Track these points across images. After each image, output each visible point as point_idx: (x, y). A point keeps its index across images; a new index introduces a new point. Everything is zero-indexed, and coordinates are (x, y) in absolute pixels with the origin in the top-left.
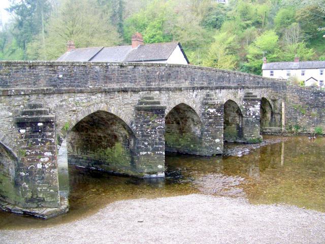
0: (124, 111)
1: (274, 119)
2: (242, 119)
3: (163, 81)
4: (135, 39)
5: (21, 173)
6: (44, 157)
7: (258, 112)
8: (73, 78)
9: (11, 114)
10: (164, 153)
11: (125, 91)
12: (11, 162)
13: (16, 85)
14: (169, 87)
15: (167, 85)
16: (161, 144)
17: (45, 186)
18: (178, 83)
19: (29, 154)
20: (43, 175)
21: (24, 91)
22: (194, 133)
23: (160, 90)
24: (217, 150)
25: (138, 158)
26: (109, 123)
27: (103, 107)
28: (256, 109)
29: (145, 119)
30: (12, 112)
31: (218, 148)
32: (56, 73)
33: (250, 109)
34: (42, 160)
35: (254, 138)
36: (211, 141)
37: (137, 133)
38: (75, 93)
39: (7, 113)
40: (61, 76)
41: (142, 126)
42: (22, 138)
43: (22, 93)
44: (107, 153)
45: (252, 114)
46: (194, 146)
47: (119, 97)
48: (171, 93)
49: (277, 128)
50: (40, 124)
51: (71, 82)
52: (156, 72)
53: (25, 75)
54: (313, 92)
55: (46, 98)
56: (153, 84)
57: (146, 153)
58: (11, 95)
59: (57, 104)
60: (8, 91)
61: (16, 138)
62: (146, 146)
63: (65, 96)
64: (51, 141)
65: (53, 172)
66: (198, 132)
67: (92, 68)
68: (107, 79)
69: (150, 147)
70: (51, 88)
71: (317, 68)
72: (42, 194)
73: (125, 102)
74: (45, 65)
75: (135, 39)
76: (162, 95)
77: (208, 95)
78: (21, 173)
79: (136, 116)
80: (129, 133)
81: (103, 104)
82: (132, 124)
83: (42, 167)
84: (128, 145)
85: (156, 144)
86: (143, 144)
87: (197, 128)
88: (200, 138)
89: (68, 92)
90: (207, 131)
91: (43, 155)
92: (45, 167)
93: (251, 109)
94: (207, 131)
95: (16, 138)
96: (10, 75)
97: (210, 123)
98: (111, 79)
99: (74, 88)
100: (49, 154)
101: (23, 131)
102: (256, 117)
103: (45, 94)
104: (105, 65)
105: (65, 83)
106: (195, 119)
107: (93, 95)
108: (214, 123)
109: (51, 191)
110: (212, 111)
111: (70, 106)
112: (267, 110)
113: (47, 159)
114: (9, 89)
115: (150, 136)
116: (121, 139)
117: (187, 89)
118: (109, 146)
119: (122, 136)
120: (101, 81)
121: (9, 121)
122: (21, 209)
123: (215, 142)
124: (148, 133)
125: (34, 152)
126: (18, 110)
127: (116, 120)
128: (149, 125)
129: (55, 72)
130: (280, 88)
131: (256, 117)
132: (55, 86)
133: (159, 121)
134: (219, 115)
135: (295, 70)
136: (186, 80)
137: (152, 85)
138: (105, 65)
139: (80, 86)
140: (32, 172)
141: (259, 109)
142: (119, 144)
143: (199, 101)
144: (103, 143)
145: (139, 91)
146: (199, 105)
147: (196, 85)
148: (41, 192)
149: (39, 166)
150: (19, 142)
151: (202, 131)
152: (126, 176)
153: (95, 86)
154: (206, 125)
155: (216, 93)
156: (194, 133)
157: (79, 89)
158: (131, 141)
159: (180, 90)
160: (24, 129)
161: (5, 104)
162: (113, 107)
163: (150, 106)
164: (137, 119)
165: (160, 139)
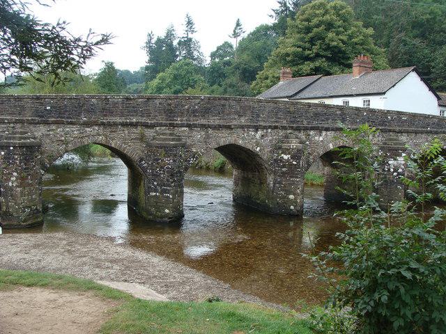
3: (195, 116)
14: (207, 123)
33: (390, 162)
34: (12, 179)
38: (63, 124)
45: (392, 170)
48: (210, 131)
50: (12, 148)
52: (183, 106)
55: (31, 127)
71: (393, 86)
76: (195, 133)
89: (54, 123)
93: (391, 162)
94: (280, 183)
97: (284, 173)
110: (286, 157)
113: (14, 178)
123: (288, 198)
147: (262, 123)
159: (229, 127)
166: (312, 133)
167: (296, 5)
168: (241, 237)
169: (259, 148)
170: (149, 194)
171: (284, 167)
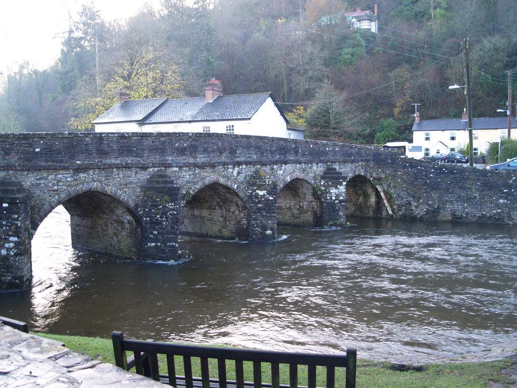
0: (125, 192)
6: (10, 242)
11: (127, 167)
27: (95, 185)
34: (7, 245)
37: (144, 219)
41: (150, 210)
45: (334, 198)
64: (17, 224)
68: (102, 153)
77: (257, 172)
81: (96, 184)
85: (168, 233)
89: (47, 169)
93: (333, 191)
97: (259, 209)
99: (56, 164)
100: (15, 239)
110: (261, 193)
111: (50, 185)
112: (369, 193)
113: (12, 245)
127: (118, 203)
129: (30, 145)
133: (171, 205)
134: (271, 198)
141: (344, 190)
155: (273, 169)
157: (62, 165)
166: (275, 167)
168: (29, 180)
169: (236, 186)
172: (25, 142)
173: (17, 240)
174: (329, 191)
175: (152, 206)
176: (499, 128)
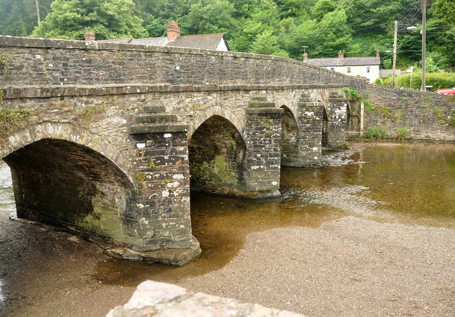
1: (350, 123)
2: (327, 123)
3: (269, 78)
4: (171, 30)
5: (138, 205)
6: (172, 180)
7: (345, 114)
8: (189, 72)
9: (125, 121)
10: (279, 167)
11: (237, 90)
12: (119, 190)
13: (131, 80)
15: (272, 84)
16: (277, 155)
17: (173, 221)
18: (281, 81)
19: (150, 177)
20: (171, 206)
21: (141, 89)
22: (288, 140)
23: (267, 89)
24: (315, 160)
25: (249, 174)
26: (212, 131)
28: (342, 111)
29: (258, 125)
30: (125, 118)
31: (316, 158)
32: (173, 64)
33: (336, 111)
34: (169, 185)
35: (339, 144)
36: (309, 150)
39: (120, 120)
40: (178, 68)
42: (140, 155)
43: (138, 91)
44: (202, 168)
45: (337, 117)
46: (287, 156)
47: (232, 97)
49: (355, 133)
50: (167, 136)
51: (188, 77)
52: (264, 66)
53: (140, 65)
54: (395, 92)
56: (261, 81)
57: (258, 167)
58: (125, 94)
59: (175, 106)
60: (122, 87)
61: (131, 156)
62: (258, 159)
63: (183, 96)
65: (185, 201)
66: (293, 139)
67: (208, 59)
69: (263, 160)
70: (167, 84)
71: (363, 65)
72: (168, 232)
73: (238, 104)
74: (162, 51)
75: (171, 30)
78: (138, 205)
79: (247, 122)
80: (237, 142)
81: (218, 107)
82: (243, 132)
83: (170, 195)
84: (235, 158)
85: (271, 156)
86: (255, 156)
87: (291, 134)
88: (296, 146)
90: (304, 138)
91: (171, 178)
92: (173, 195)
93: (337, 111)
94: (304, 138)
95: (131, 156)
96: (124, 63)
97: (308, 129)
98: (225, 74)
101: (141, 146)
102: (342, 120)
103: (161, 93)
104: (221, 54)
105: (182, 78)
106: (290, 124)
107: (209, 95)
108: (312, 128)
109: (181, 226)
110: (309, 114)
113: (176, 184)
114: (123, 85)
115: (264, 146)
116: (224, 150)
117: (288, 88)
118: (206, 160)
119: (226, 147)
120: (217, 76)
121: (123, 132)
122: (138, 253)
124: (261, 143)
125: (157, 175)
126: (132, 116)
128: (262, 133)
130: (359, 87)
131: (342, 120)
132: (172, 81)
135: (340, 67)
136: (287, 77)
137: (260, 83)
138: (221, 54)
139: (196, 83)
140: (154, 202)
141: (346, 111)
142: (221, 156)
143: (296, 103)
144: (197, 156)
145: (250, 90)
146: (297, 108)
148: (167, 228)
149: (165, 194)
150: (135, 161)
151: (298, 138)
152: (232, 196)
153: (211, 82)
154: (303, 131)
156: (288, 140)
158: (239, 152)
160: (143, 143)
161: (118, 107)
162: (227, 111)
163: (264, 108)
164: (249, 125)
165: (275, 150)
167: (451, 37)
170: (250, 168)
171: (308, 123)
172: (168, 58)
173: (183, 178)
174: (334, 112)
175: (256, 129)
176: (366, 65)
